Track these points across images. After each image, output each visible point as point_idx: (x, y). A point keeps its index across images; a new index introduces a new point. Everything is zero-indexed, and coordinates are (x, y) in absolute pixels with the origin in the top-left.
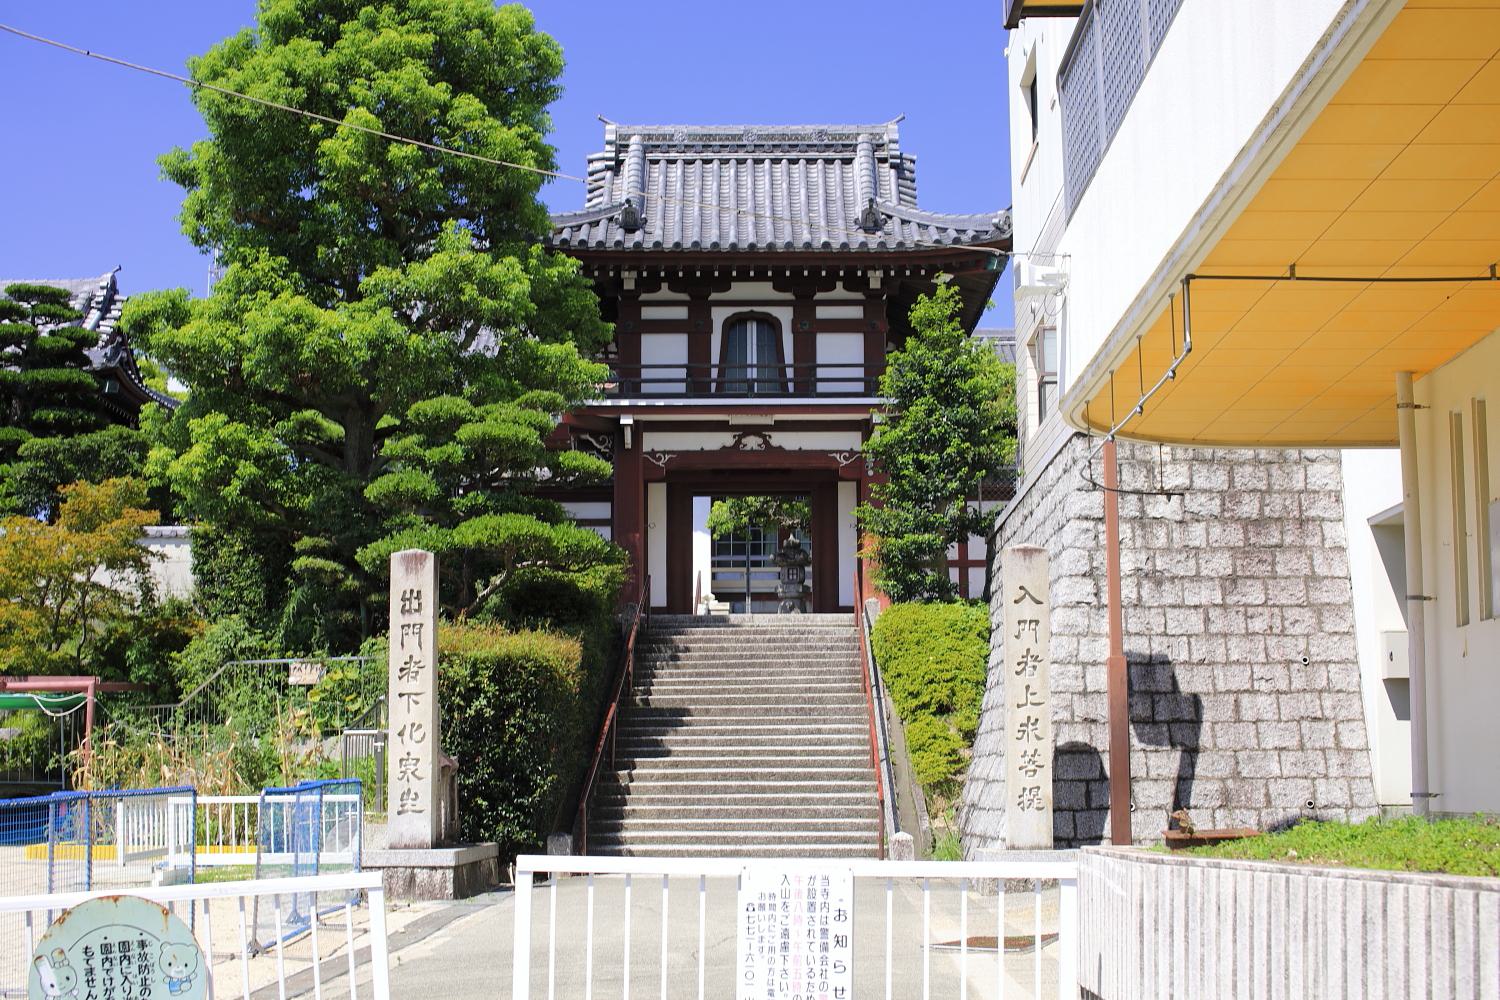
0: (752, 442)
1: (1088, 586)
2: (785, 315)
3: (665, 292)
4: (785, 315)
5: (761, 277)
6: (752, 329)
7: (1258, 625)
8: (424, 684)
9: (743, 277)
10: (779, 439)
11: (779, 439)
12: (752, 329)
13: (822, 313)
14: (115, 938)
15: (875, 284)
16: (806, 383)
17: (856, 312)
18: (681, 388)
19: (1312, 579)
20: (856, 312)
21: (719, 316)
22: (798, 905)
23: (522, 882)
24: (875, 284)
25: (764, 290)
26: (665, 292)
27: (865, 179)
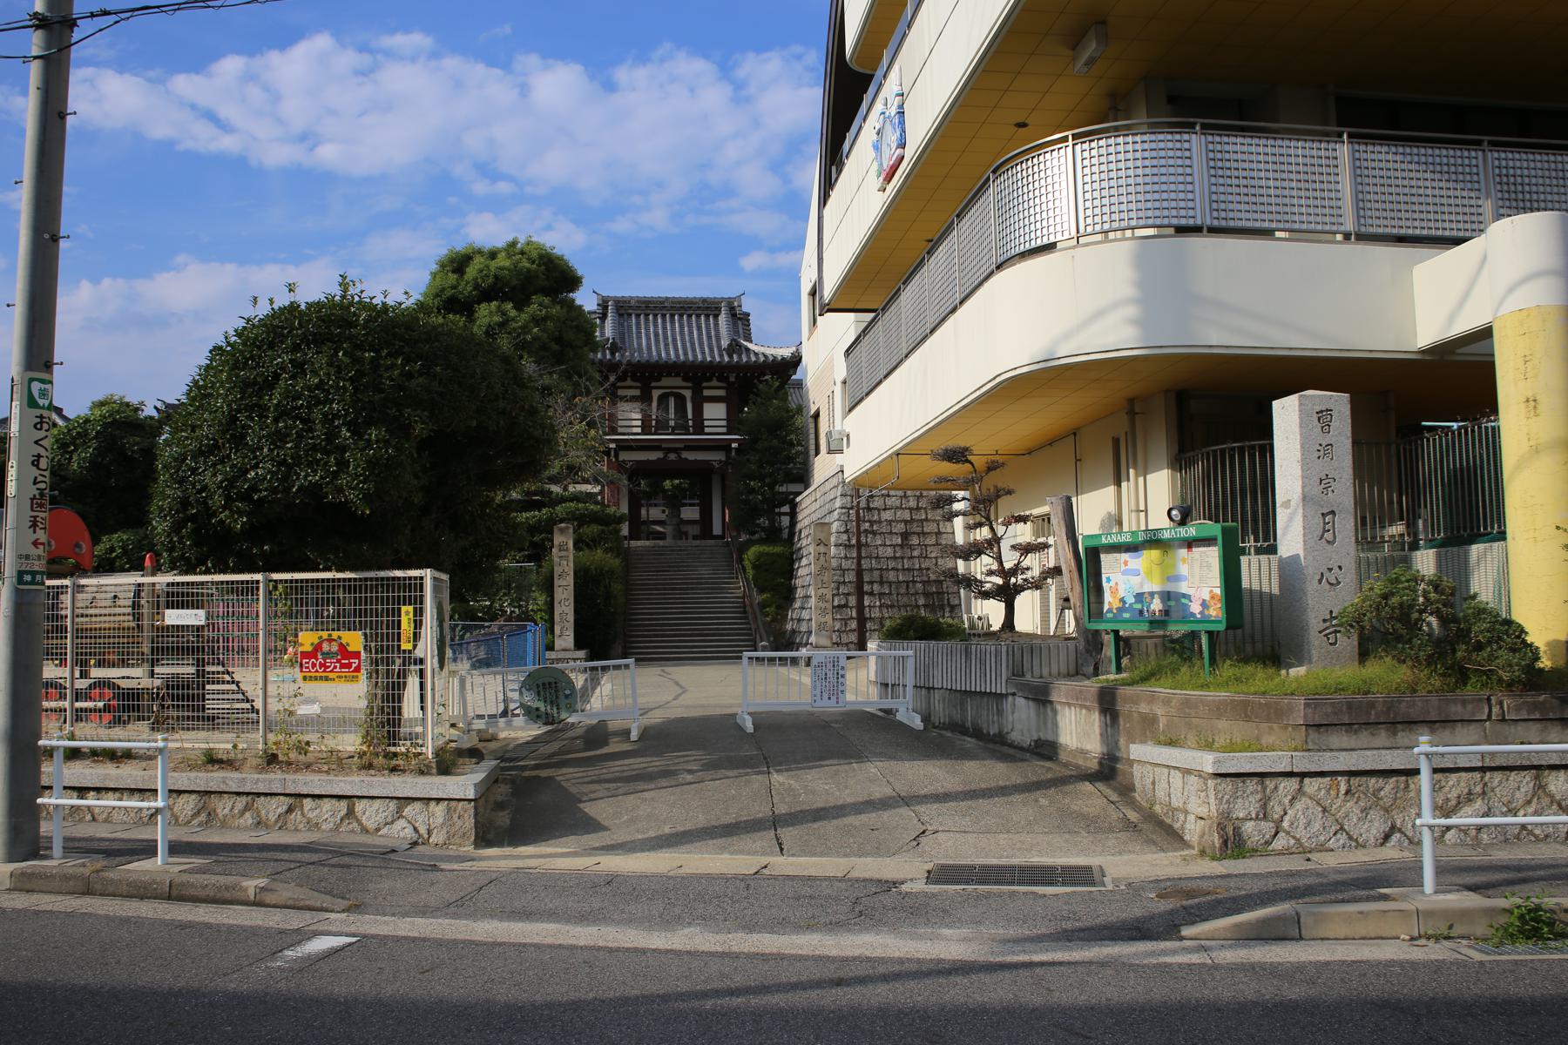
0: (672, 456)
1: (845, 537)
2: (688, 394)
3: (629, 382)
4: (688, 394)
5: (677, 375)
6: (672, 401)
7: (916, 553)
8: (570, 580)
9: (669, 375)
10: (685, 455)
11: (685, 455)
12: (672, 401)
13: (706, 393)
14: (547, 680)
15: (732, 379)
16: (699, 427)
17: (721, 393)
18: (639, 430)
19: (939, 533)
20: (721, 393)
21: (656, 394)
22: (830, 666)
23: (745, 660)
24: (732, 379)
25: (678, 381)
26: (629, 382)
27: (1161, 794)
